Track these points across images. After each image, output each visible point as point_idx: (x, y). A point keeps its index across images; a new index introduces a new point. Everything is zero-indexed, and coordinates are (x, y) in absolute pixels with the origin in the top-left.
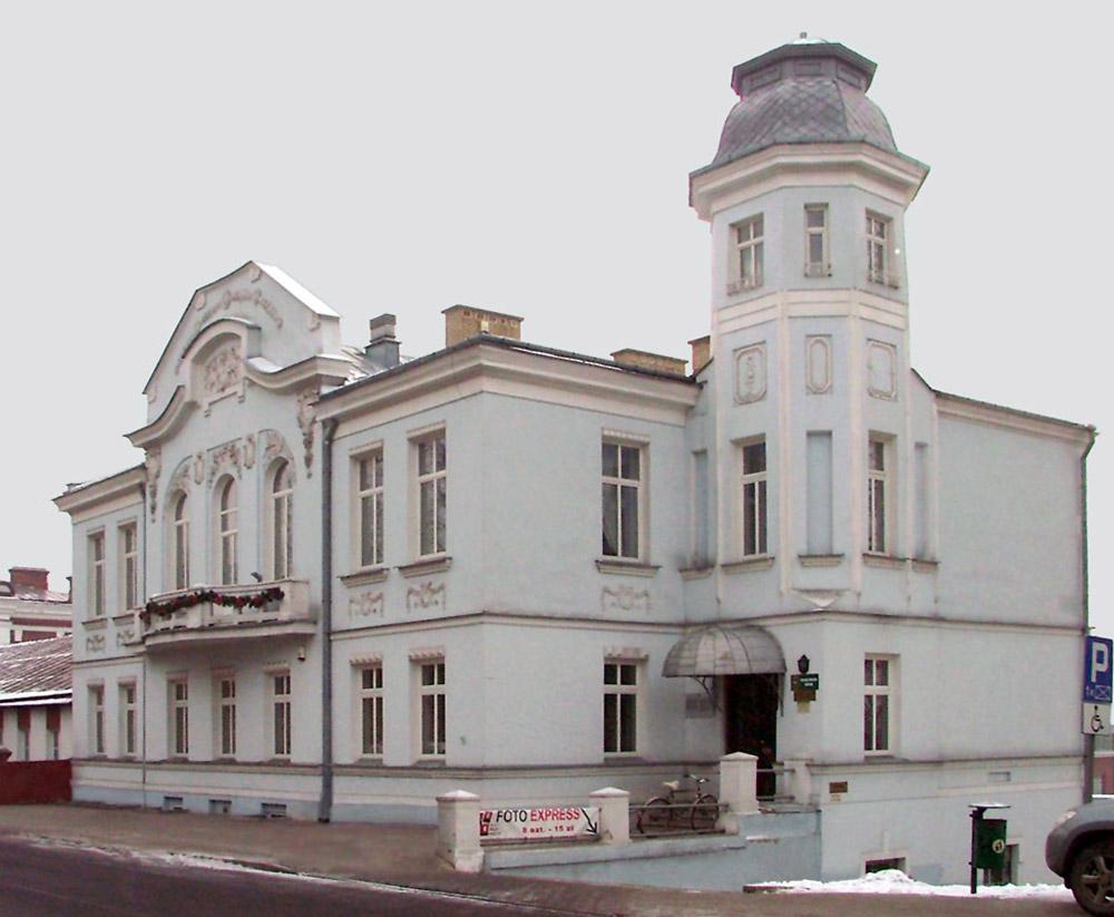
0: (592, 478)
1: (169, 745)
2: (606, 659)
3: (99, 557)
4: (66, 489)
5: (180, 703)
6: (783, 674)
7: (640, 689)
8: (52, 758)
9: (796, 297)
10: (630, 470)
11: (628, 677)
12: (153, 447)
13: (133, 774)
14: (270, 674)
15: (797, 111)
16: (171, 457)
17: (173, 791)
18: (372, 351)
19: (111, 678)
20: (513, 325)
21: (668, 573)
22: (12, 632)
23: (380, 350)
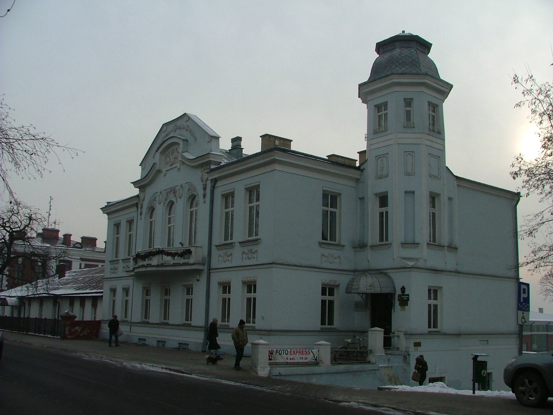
0: (318, 207)
4: (106, 204)
6: (395, 294)
7: (338, 298)
8: (93, 319)
9: (400, 135)
11: (331, 293)
14: (185, 286)
16: (150, 192)
19: (119, 285)
22: (80, 264)
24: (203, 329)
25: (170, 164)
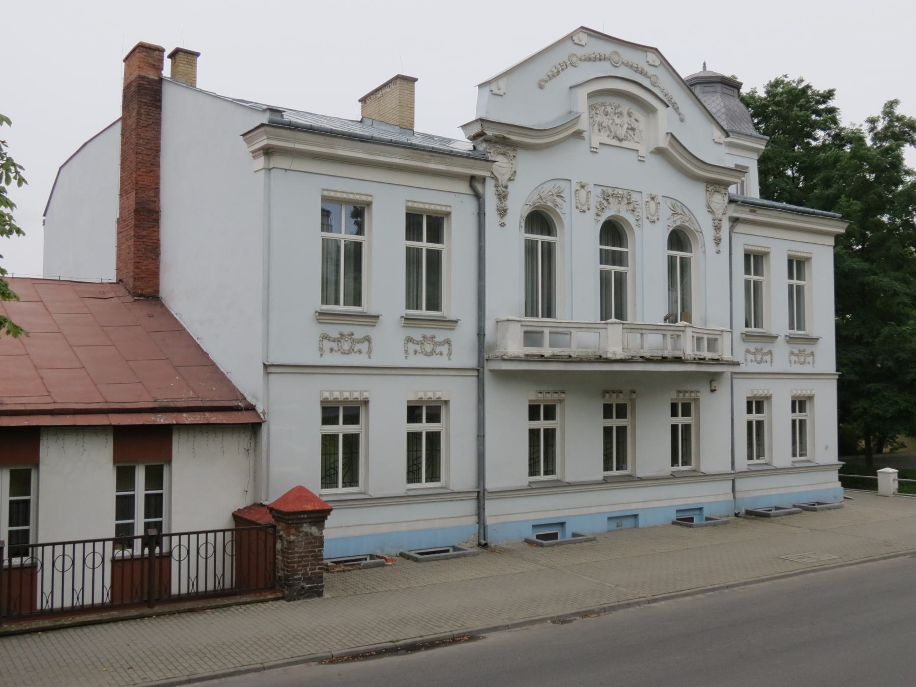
2: (322, 402)
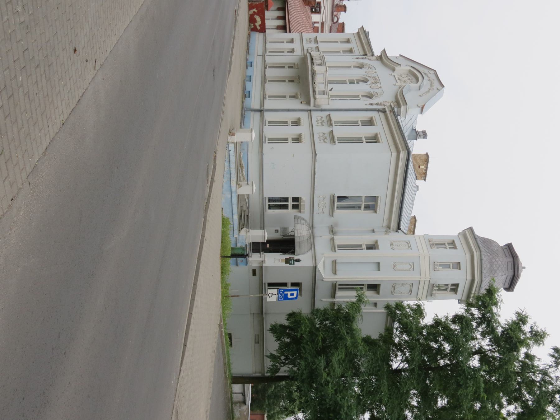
0: (364, 193)
1: (271, 63)
3: (341, 42)
4: (367, 31)
5: (286, 67)
7: (290, 212)
8: (266, 18)
9: (427, 259)
10: (367, 207)
11: (295, 207)
12: (380, 58)
13: (260, 52)
14: (297, 94)
15: (494, 261)
16: (377, 64)
17: (254, 64)
18: (414, 131)
19: (296, 46)
20: (423, 178)
21: (331, 221)
22: (318, 22)
23: (414, 133)
24: (262, 108)
25: (400, 78)
